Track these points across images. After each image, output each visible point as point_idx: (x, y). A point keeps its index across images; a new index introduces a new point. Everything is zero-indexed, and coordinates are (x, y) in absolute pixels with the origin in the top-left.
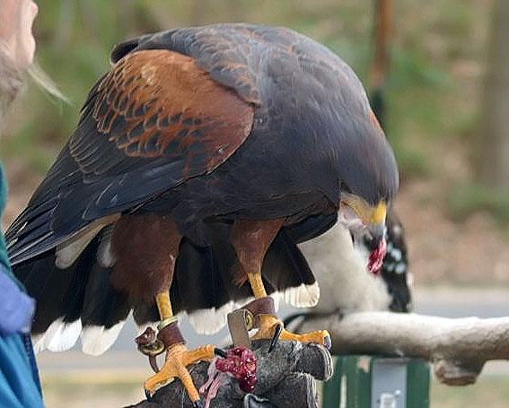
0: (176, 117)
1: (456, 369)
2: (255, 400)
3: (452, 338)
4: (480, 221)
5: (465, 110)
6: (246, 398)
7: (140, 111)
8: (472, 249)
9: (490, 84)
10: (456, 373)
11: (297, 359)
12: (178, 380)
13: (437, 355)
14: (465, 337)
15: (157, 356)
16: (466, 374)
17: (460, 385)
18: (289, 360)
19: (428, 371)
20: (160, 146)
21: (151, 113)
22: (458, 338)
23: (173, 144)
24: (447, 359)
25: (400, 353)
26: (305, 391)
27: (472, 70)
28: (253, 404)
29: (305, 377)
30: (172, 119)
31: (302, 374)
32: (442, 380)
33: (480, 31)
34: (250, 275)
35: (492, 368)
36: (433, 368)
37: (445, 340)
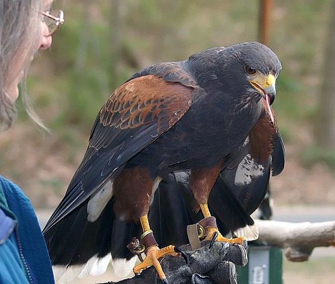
0: (149, 102)
1: (297, 253)
2: (199, 277)
3: (295, 235)
4: (319, 168)
5: (310, 104)
6: (193, 275)
7: (128, 105)
8: (315, 184)
9: (325, 89)
10: (297, 254)
11: (225, 253)
12: (153, 267)
13: (286, 245)
14: (301, 234)
15: (142, 254)
16: (302, 255)
17: (299, 261)
18: (220, 253)
19: (281, 254)
20: (142, 119)
21: (134, 104)
22: (298, 234)
23: (150, 115)
24: (292, 247)
25: (265, 243)
26: (229, 272)
27: (314, 81)
28: (198, 280)
29: (229, 264)
30: (147, 103)
31: (227, 262)
32: (289, 258)
33: (319, 58)
34: (201, 205)
35: (318, 252)
36: (285, 251)
37: (291, 236)
